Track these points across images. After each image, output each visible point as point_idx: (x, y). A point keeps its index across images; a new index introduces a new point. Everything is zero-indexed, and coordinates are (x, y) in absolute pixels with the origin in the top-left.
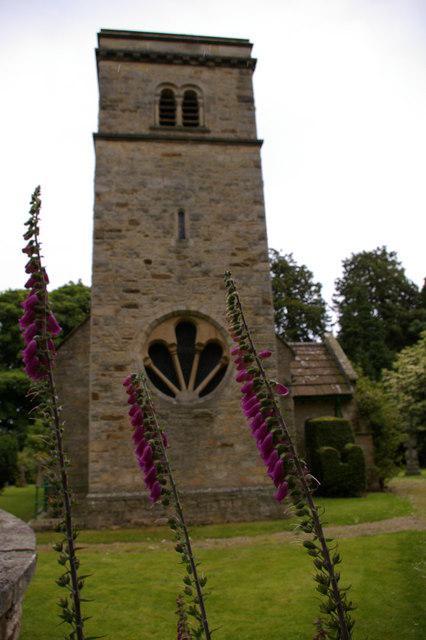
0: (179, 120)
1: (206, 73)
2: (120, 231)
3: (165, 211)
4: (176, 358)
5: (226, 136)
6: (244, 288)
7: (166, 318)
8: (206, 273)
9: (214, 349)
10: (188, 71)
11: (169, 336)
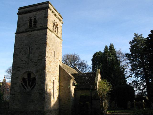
0: (32, 26)
1: (38, 13)
2: (18, 54)
3: (26, 48)
4: (27, 82)
5: (41, 28)
6: (40, 65)
7: (25, 73)
8: (32, 62)
9: (34, 79)
10: (35, 13)
11: (26, 77)
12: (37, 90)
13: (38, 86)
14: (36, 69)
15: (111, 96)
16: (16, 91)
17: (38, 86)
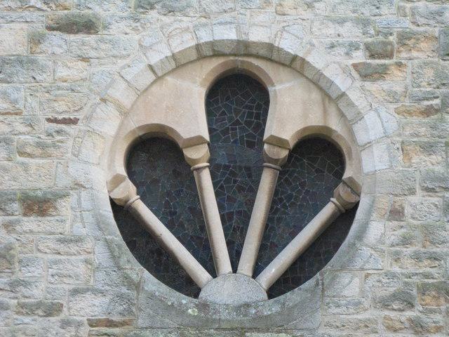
7: (179, 64)
9: (320, 154)
11: (190, 120)
12: (385, 303)
13: (406, 241)
14: (365, 23)
15: (200, 310)
16: (52, 310)
17: (406, 241)
